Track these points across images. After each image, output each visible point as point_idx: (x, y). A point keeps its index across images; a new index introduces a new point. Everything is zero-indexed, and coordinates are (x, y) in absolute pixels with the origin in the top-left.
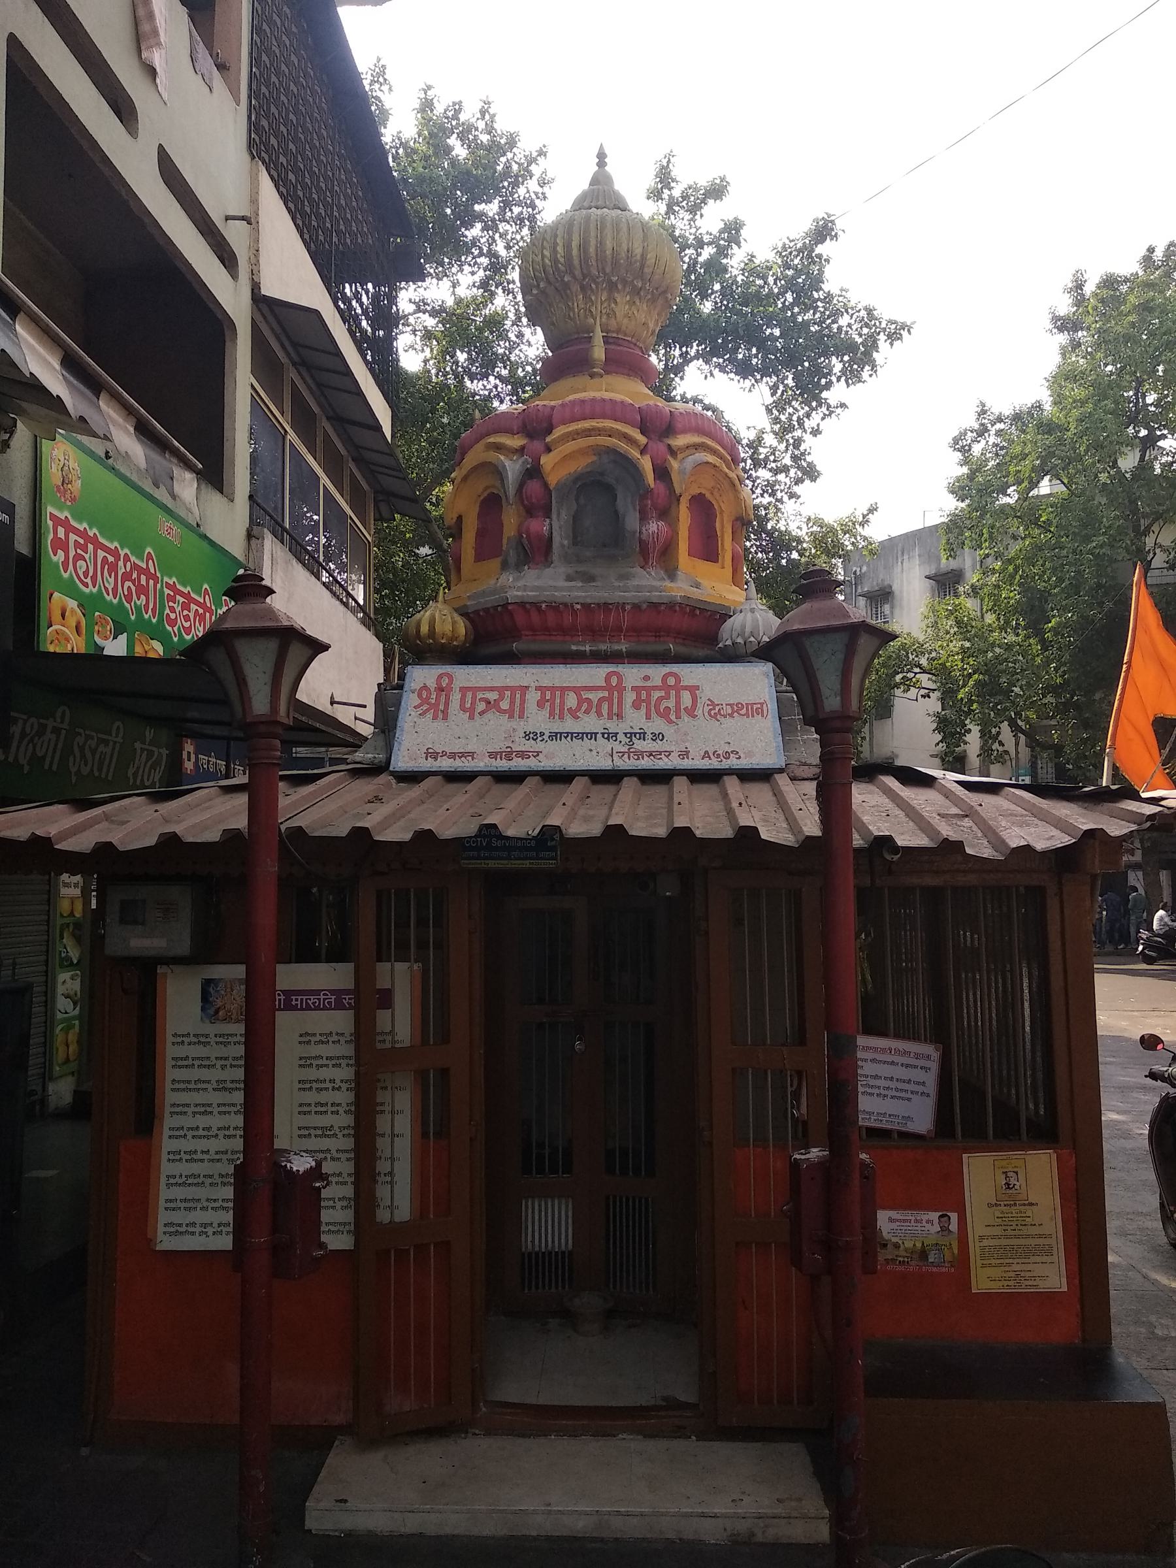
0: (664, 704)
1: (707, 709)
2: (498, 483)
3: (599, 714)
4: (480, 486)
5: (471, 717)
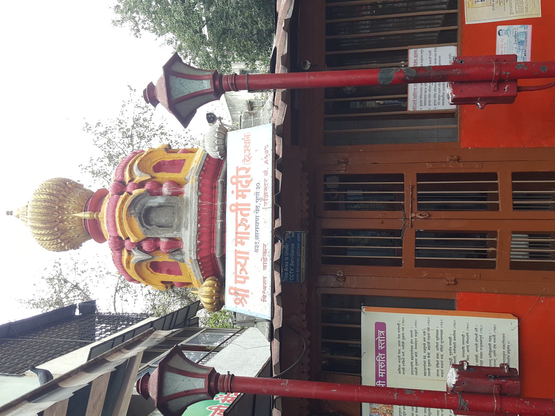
0: (244, 183)
1: (246, 162)
2: (145, 263)
3: (248, 215)
4: (148, 272)
5: (248, 278)
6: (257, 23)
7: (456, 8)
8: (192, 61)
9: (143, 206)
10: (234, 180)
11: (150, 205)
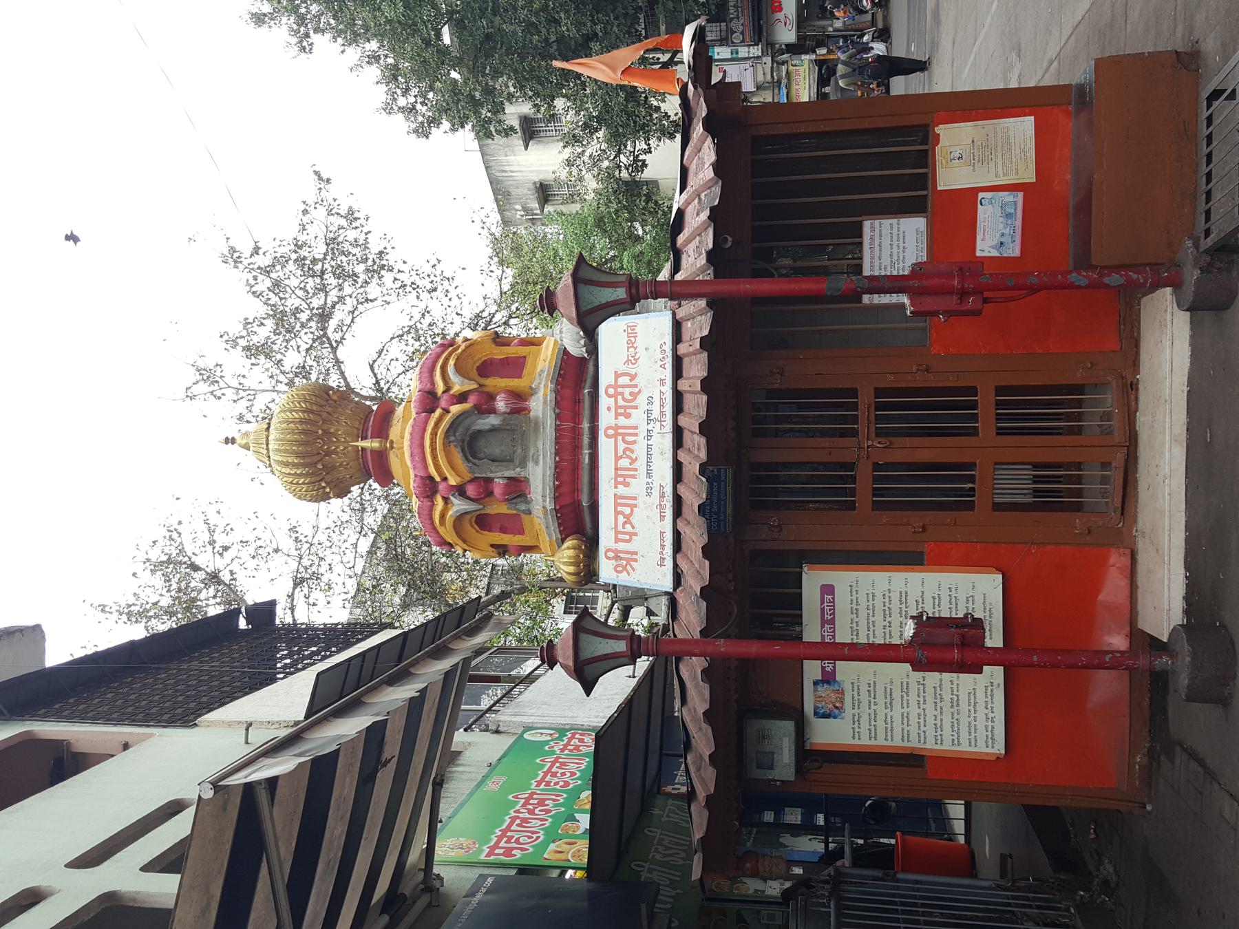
0: (627, 396)
2: (468, 517)
3: (634, 442)
4: (470, 530)
5: (636, 534)
6: (557, 22)
7: (925, 189)
8: (419, 100)
9: (468, 429)
10: (611, 391)
11: (478, 428)
